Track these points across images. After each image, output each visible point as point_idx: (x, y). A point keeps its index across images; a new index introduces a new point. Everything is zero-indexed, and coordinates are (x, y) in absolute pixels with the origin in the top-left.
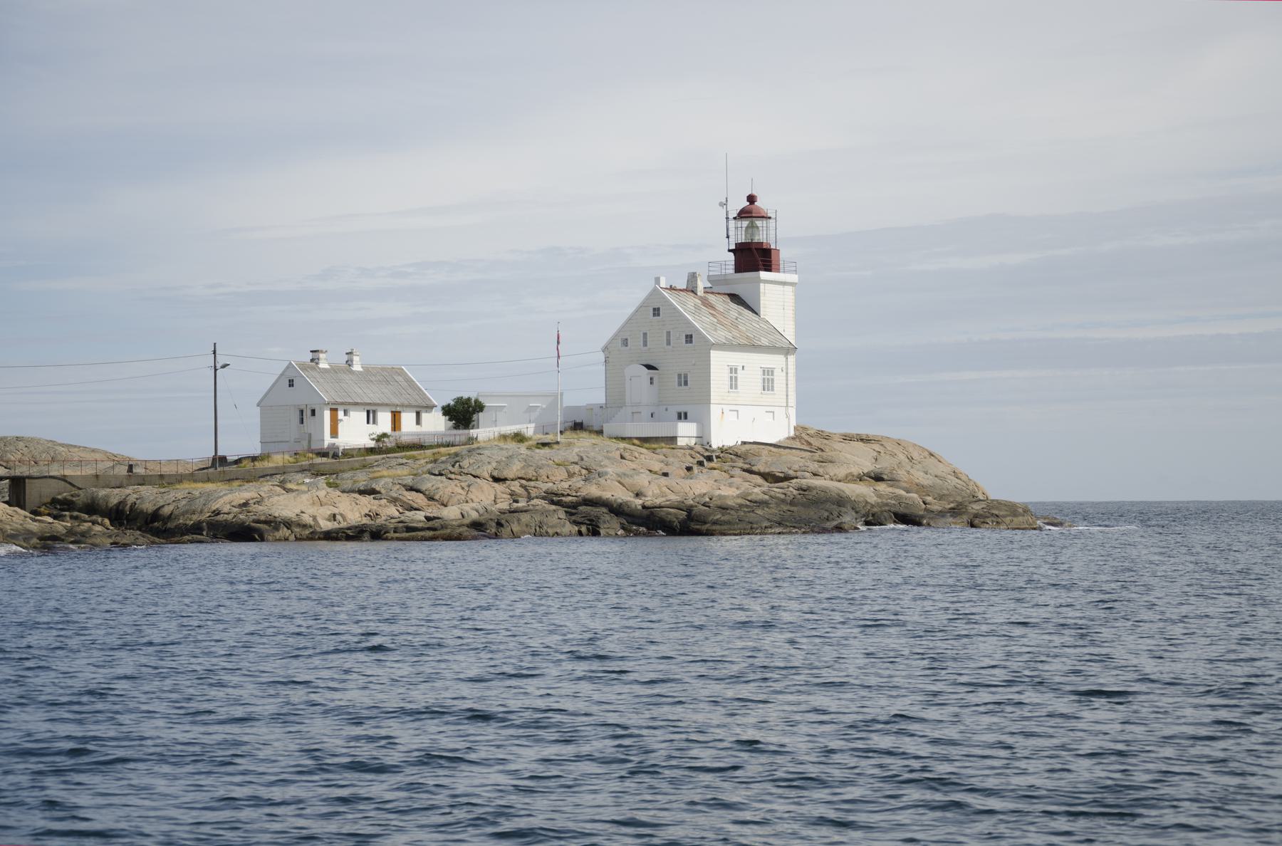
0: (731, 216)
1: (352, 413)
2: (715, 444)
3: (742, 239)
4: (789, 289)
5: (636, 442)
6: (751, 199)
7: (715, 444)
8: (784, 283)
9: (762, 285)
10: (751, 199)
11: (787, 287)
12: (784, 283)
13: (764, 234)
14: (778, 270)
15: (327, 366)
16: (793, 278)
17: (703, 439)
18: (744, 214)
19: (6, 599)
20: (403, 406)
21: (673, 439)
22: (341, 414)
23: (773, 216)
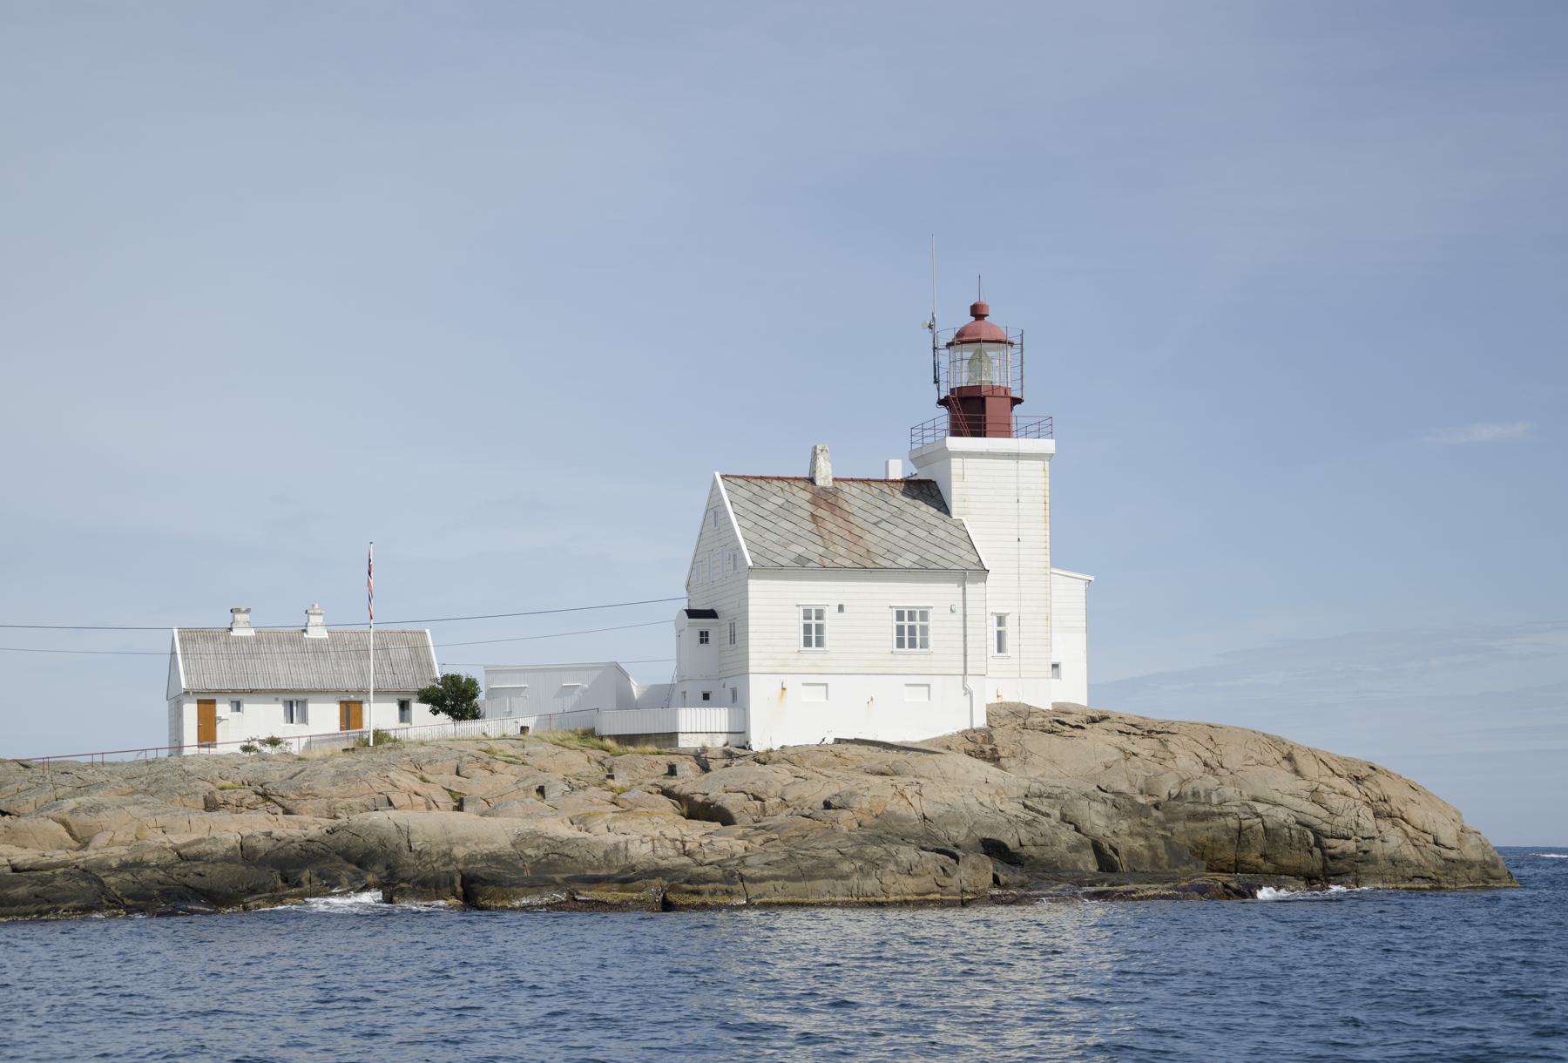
0: (942, 343)
1: (246, 707)
2: (758, 744)
3: (964, 380)
4: (1039, 464)
5: (609, 743)
6: (978, 312)
7: (758, 744)
8: (1018, 456)
9: (956, 463)
10: (978, 312)
11: (1023, 464)
12: (1018, 456)
13: (997, 372)
14: (1006, 432)
15: (251, 633)
16: (1047, 445)
17: (740, 734)
18: (962, 339)
19: (1560, 893)
20: (244, 692)
21: (672, 737)
22: (223, 709)
23: (1017, 341)
